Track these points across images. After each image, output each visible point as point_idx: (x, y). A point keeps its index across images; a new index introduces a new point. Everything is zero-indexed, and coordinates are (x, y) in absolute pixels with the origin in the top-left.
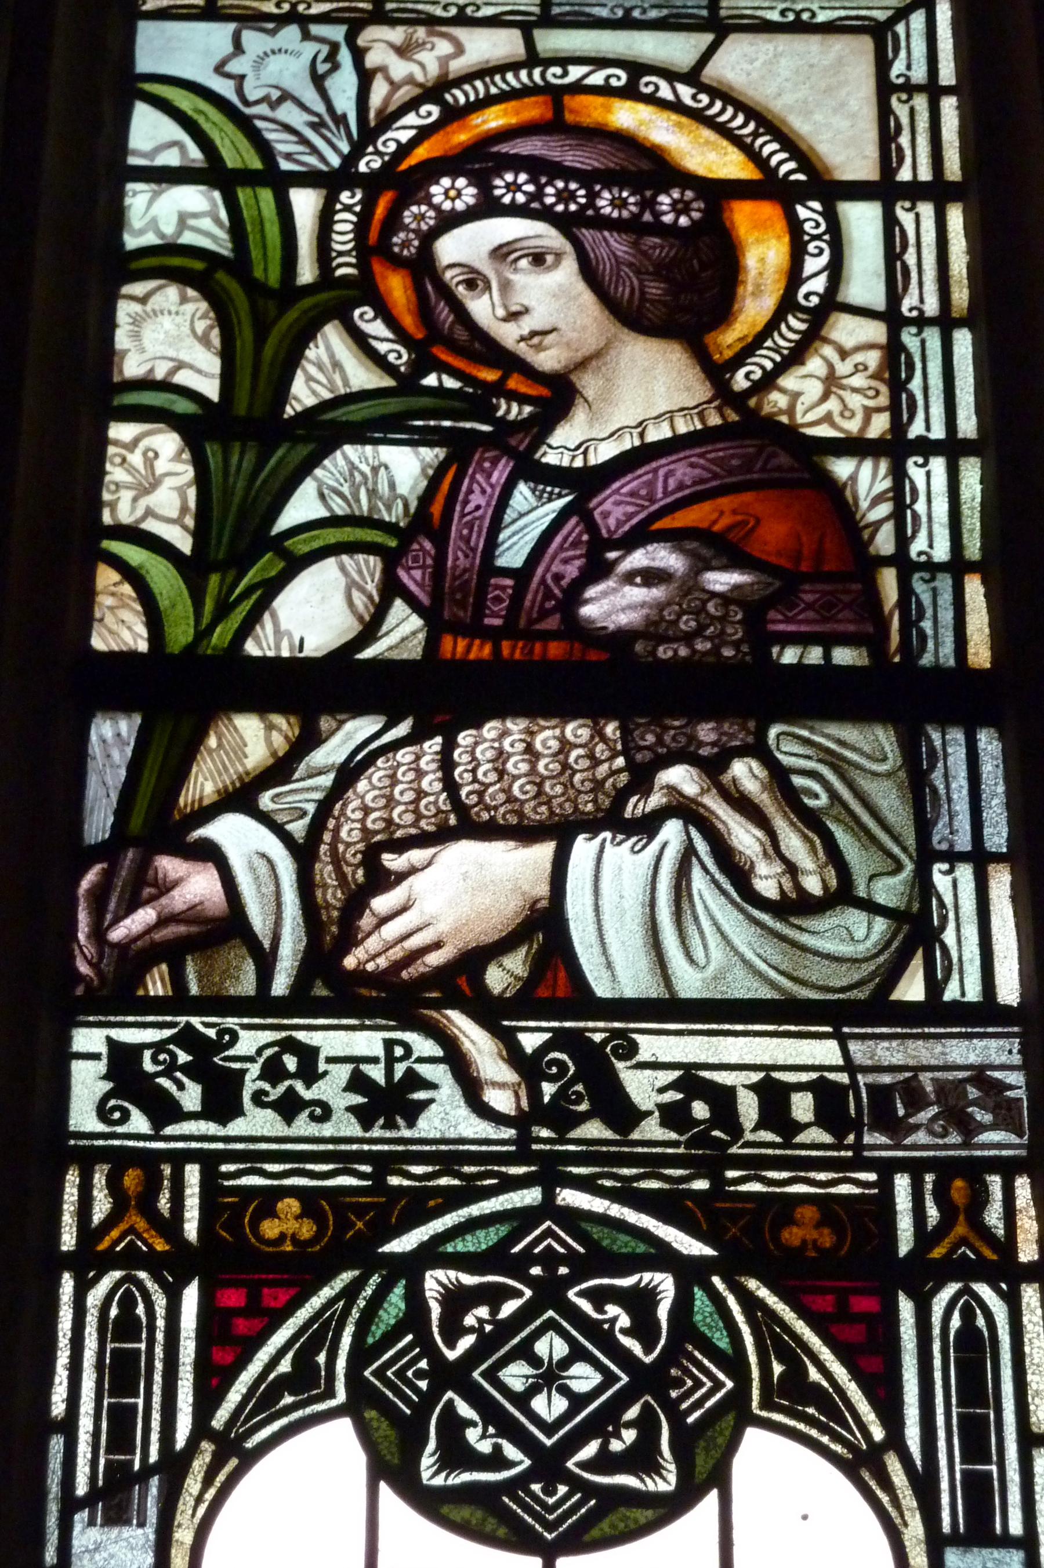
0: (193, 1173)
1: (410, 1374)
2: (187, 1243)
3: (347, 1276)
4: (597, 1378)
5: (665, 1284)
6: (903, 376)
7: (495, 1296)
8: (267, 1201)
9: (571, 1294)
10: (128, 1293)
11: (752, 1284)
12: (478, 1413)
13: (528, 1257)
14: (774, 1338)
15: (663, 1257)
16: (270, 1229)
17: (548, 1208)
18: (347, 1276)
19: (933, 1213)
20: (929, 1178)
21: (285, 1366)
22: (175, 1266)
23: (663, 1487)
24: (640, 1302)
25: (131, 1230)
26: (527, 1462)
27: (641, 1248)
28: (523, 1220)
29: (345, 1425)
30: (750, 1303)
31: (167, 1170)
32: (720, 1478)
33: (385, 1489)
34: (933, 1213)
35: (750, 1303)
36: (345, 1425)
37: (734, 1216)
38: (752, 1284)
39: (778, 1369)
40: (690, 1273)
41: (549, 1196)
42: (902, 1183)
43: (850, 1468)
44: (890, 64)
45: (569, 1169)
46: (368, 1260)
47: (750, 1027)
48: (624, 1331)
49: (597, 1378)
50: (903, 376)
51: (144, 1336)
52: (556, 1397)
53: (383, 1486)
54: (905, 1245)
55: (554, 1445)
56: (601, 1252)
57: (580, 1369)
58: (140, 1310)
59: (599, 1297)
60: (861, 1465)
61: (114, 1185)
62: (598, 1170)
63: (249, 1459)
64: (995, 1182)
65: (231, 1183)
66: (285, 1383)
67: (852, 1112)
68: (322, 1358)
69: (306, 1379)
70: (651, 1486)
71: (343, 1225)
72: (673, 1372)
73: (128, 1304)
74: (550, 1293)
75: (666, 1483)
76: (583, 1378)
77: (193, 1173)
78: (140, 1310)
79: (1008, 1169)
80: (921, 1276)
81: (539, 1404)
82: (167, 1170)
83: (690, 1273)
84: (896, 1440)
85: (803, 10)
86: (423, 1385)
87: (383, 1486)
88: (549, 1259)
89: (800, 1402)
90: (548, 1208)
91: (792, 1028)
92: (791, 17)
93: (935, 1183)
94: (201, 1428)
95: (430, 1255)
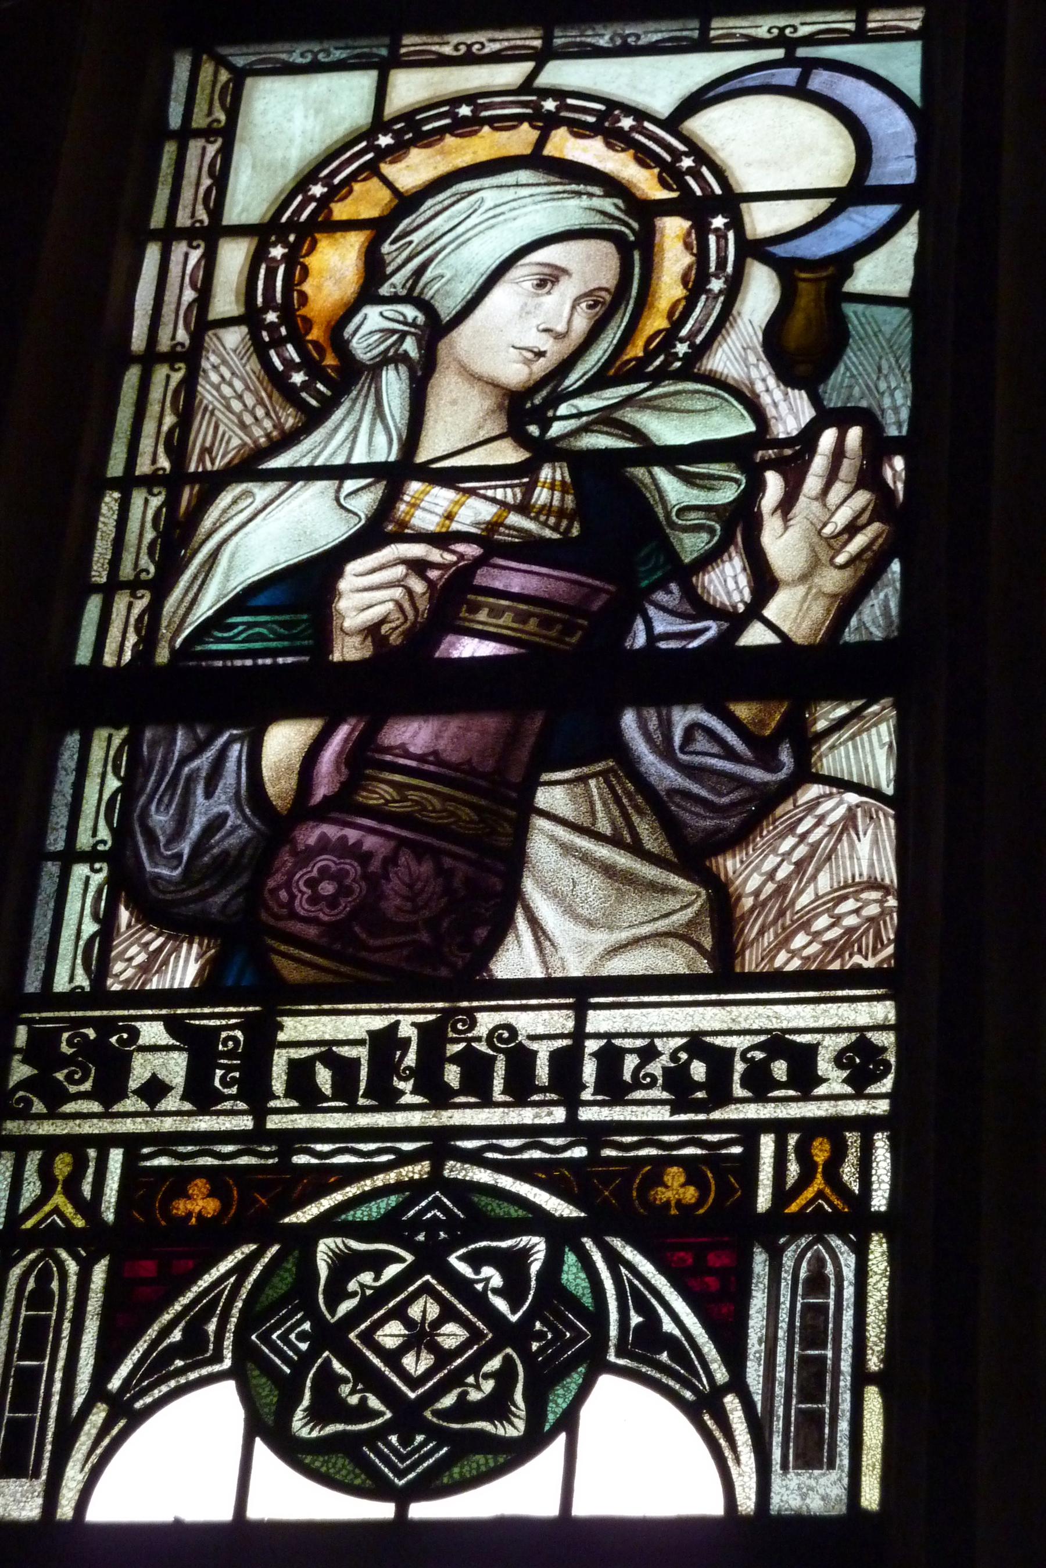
0: (116, 1157)
1: (292, 1337)
2: (104, 1223)
3: (248, 1249)
4: (462, 1334)
5: (539, 1246)
6: (164, 510)
7: (377, 1262)
8: (179, 1181)
9: (453, 1260)
10: (47, 1268)
11: (617, 1243)
12: (455, 1388)
13: (417, 1224)
14: (637, 1296)
15: (538, 1220)
16: (181, 1207)
17: (436, 1180)
18: (248, 1249)
19: (793, 1169)
20: (793, 1139)
21: (177, 1335)
22: (92, 1241)
23: (512, 1432)
24: (513, 1265)
25: (56, 1210)
26: (389, 1415)
27: (393, 1200)
28: (415, 1189)
29: (229, 1387)
30: (614, 1259)
31: (92, 1153)
32: (569, 1423)
33: (260, 1447)
34: (793, 1169)
35: (614, 1259)
36: (229, 1387)
37: (607, 1179)
38: (617, 1243)
39: (635, 1319)
40: (561, 1235)
41: (437, 1168)
42: (767, 1144)
43: (692, 1411)
44: (203, 256)
45: (704, 1152)
46: (266, 1230)
47: (723, 997)
48: (377, 1278)
49: (462, 1334)
50: (164, 510)
51: (278, 1342)
52: (424, 1354)
53: (259, 1443)
54: (764, 1200)
55: (418, 1397)
56: (479, 1217)
57: (450, 1328)
58: (55, 1285)
59: (475, 1260)
60: (703, 1409)
61: (45, 1172)
62: (484, 1142)
63: (137, 1419)
64: (852, 1138)
65: (148, 1164)
66: (175, 1351)
67: (222, 1061)
68: (212, 1327)
69: (195, 1348)
70: (501, 1432)
71: (246, 1201)
72: (538, 1325)
73: (44, 1278)
74: (430, 1258)
75: (515, 1429)
76: (452, 1335)
77: (116, 1157)
78: (55, 1285)
79: (867, 1125)
80: (774, 1230)
81: (408, 1361)
82: (92, 1153)
83: (561, 1235)
84: (738, 1384)
85: (629, 35)
86: (304, 1346)
87: (259, 1443)
88: (434, 1225)
89: (652, 1354)
90: (436, 1180)
91: (556, 1001)
92: (619, 42)
93: (798, 1142)
94: (98, 1391)
95: (326, 1225)
